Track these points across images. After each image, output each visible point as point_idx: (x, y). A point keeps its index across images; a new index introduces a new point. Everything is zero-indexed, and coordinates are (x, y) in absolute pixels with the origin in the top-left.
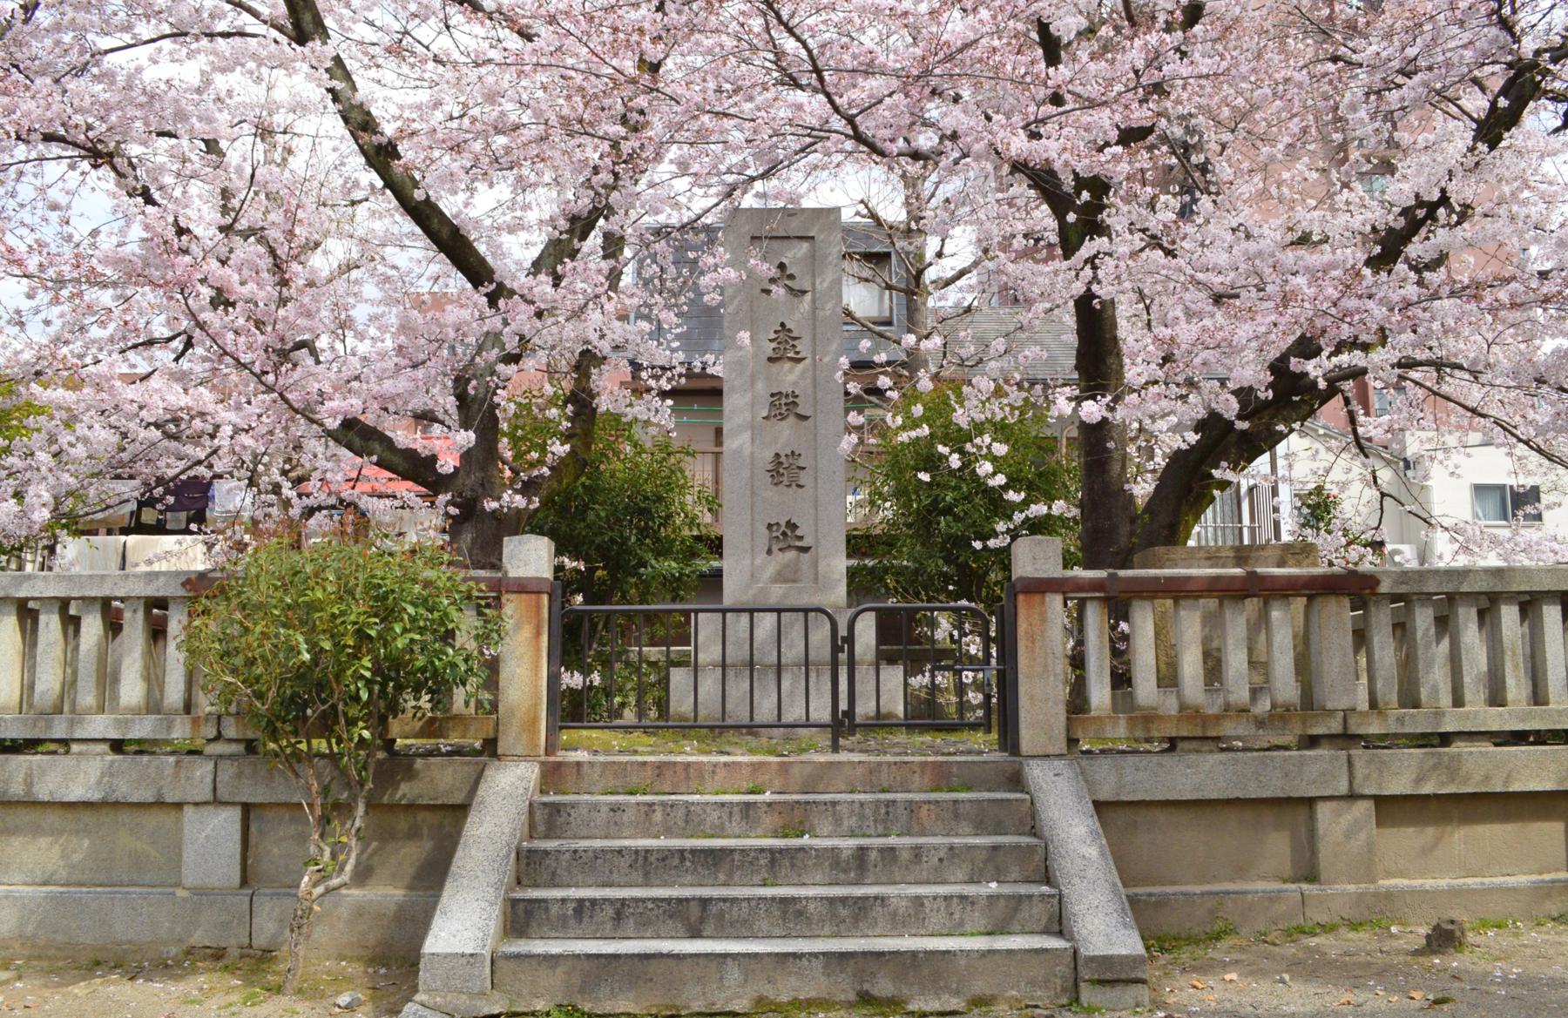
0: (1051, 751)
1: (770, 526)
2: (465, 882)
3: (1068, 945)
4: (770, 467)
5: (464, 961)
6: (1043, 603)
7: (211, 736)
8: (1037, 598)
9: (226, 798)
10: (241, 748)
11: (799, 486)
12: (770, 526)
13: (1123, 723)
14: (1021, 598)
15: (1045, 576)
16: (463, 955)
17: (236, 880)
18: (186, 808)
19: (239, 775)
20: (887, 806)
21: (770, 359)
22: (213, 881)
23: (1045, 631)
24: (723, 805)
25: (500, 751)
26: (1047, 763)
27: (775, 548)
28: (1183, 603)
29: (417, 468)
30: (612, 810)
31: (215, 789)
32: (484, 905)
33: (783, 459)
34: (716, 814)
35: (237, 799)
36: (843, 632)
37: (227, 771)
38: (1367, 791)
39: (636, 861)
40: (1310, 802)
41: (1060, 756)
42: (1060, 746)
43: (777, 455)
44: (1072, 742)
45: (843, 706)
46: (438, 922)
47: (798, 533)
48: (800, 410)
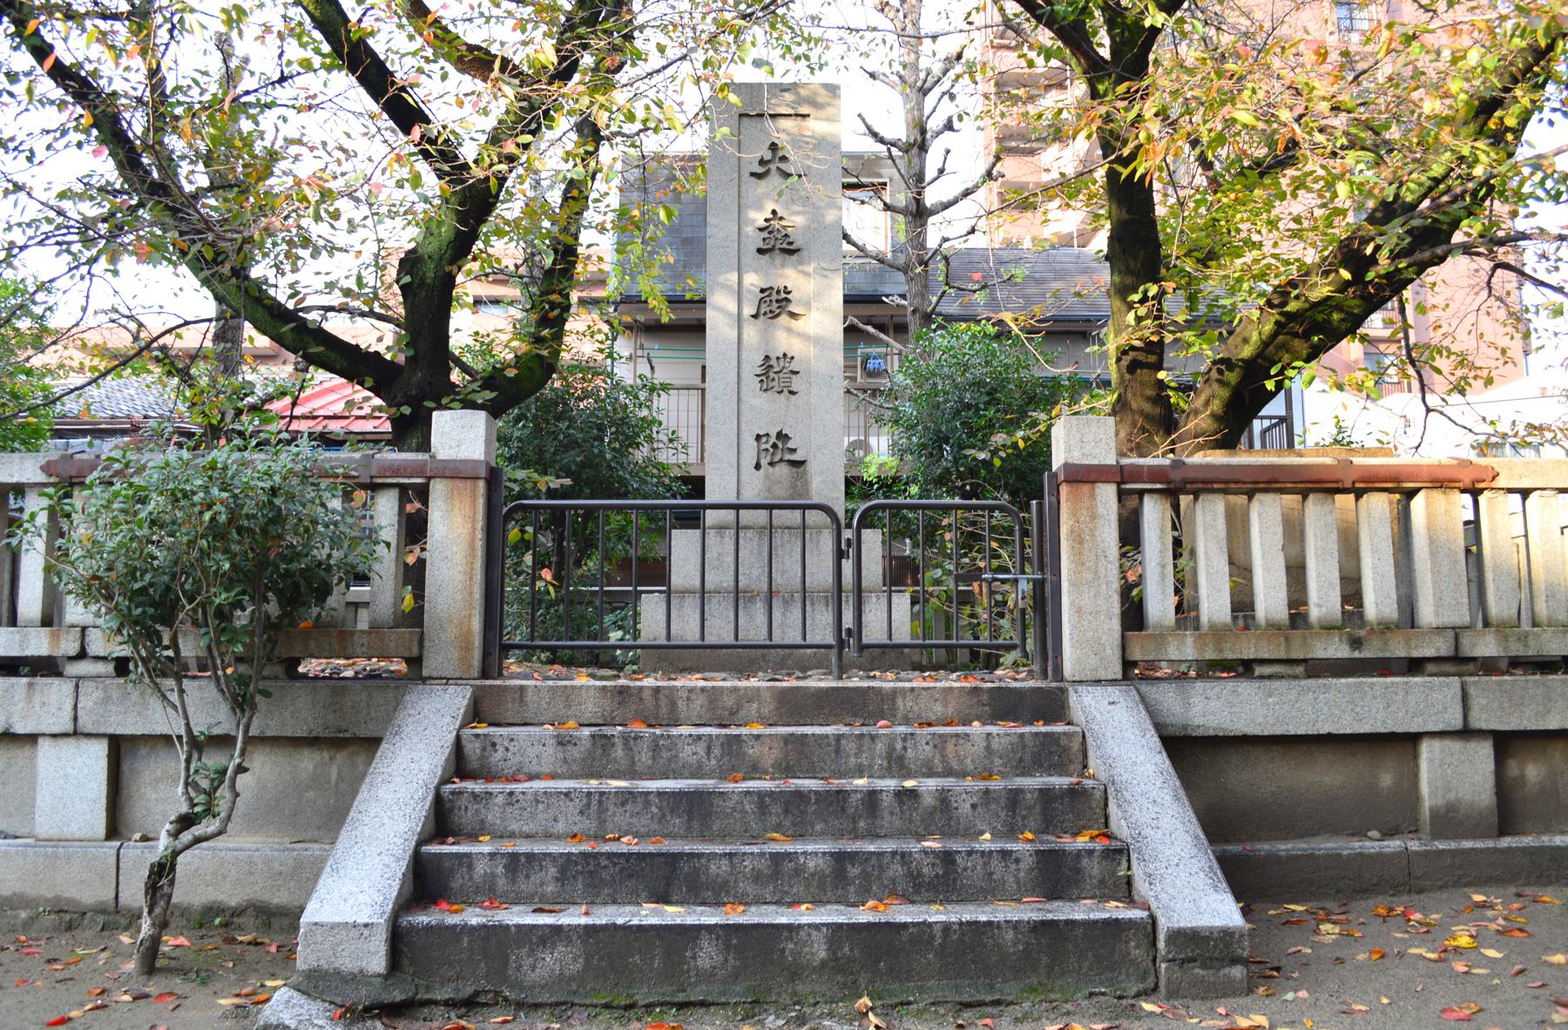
0: (1102, 675)
1: (758, 437)
2: (367, 831)
3: (1145, 914)
4: (759, 371)
5: (354, 933)
6: (1093, 496)
7: (72, 653)
8: (1086, 488)
9: (89, 728)
10: (110, 668)
11: (792, 393)
12: (758, 437)
13: (1189, 641)
14: (1064, 489)
15: (1096, 462)
16: (355, 926)
17: (101, 830)
18: (41, 740)
19: (106, 700)
20: (904, 740)
21: (760, 251)
22: (73, 830)
23: (1086, 529)
24: (699, 737)
25: (425, 673)
26: (1099, 690)
27: (764, 462)
28: (1258, 496)
29: (352, 363)
30: (560, 743)
31: (75, 719)
32: (387, 860)
33: (773, 362)
34: (689, 750)
35: (102, 730)
36: (928, 85)
37: (91, 697)
38: (1484, 726)
39: (588, 805)
40: (1411, 740)
41: (1113, 682)
42: (1116, 670)
43: (767, 358)
44: (1128, 665)
45: (848, 620)
46: (326, 882)
47: (790, 445)
48: (792, 308)
